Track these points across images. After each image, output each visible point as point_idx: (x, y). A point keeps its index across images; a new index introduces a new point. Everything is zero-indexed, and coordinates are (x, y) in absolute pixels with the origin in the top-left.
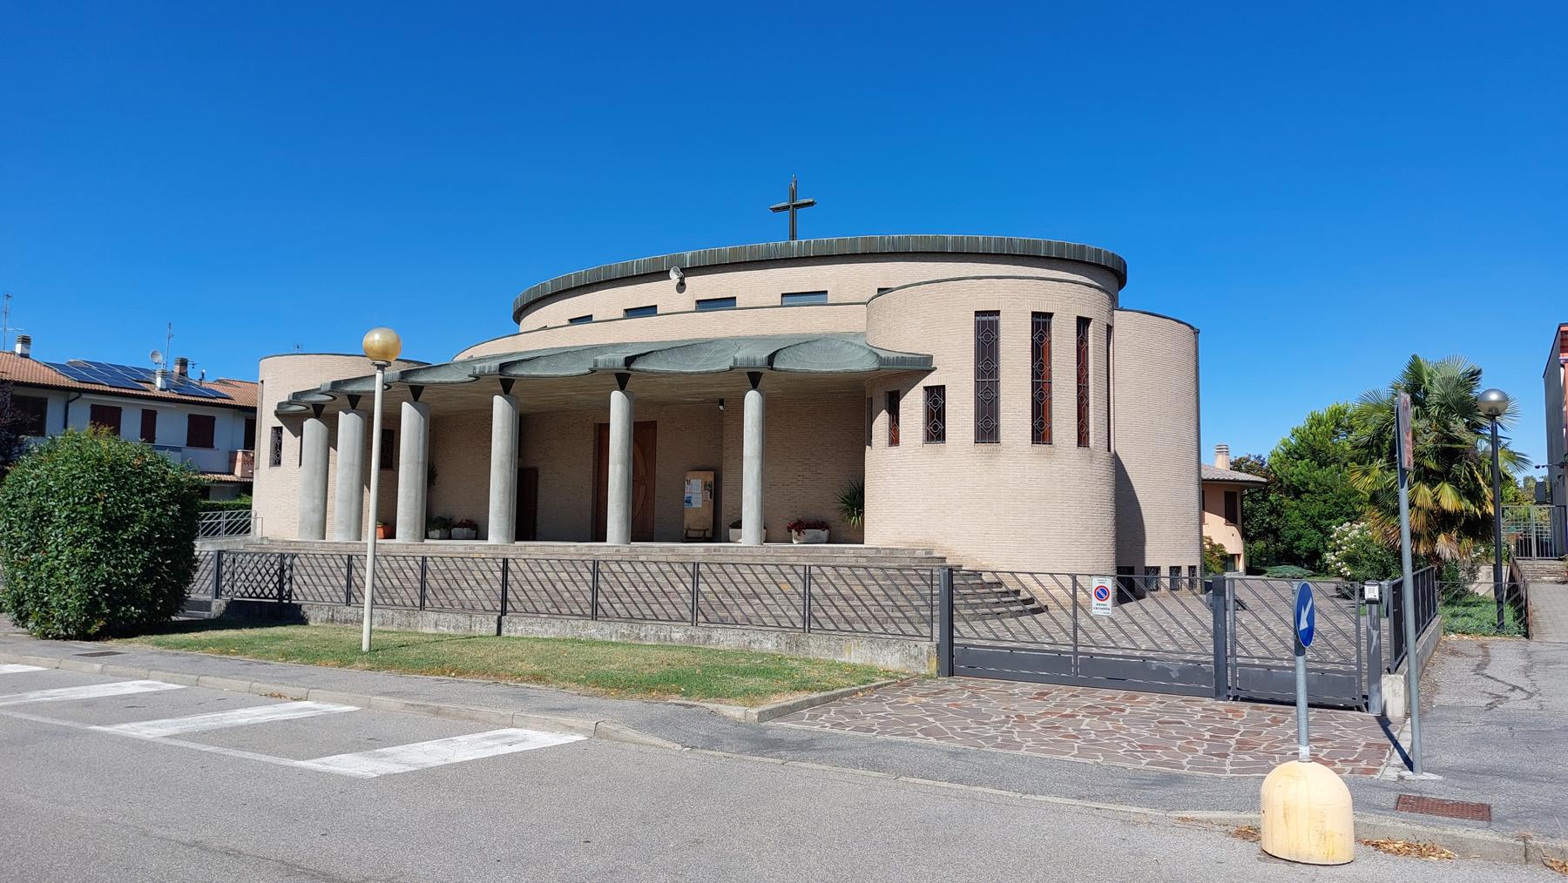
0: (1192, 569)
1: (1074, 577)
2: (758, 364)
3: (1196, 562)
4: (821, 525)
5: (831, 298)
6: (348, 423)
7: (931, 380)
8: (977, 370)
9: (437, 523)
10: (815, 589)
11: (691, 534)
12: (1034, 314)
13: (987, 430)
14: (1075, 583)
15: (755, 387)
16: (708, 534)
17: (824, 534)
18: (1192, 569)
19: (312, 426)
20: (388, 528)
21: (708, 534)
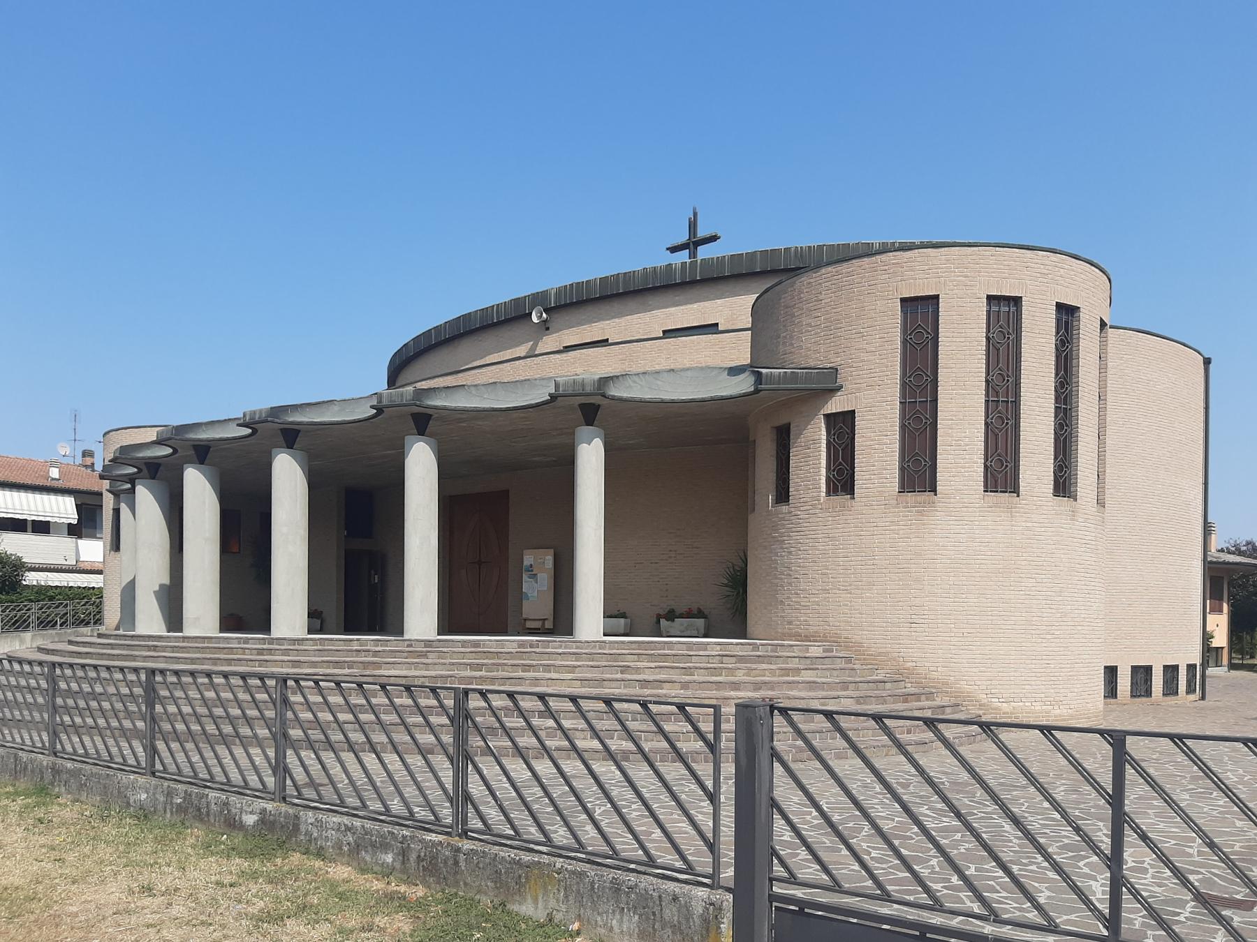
0: (1191, 668)
1: (1117, 740)
2: (588, 389)
3: (1197, 660)
4: (700, 614)
5: (720, 328)
6: (199, 490)
7: (835, 405)
8: (904, 385)
9: (474, 601)
10: (475, 788)
11: (529, 625)
12: (990, 298)
13: (919, 473)
14: (1121, 758)
15: (589, 422)
16: (549, 625)
17: (700, 622)
18: (1191, 668)
19: (145, 497)
20: (246, 605)
21: (549, 625)
